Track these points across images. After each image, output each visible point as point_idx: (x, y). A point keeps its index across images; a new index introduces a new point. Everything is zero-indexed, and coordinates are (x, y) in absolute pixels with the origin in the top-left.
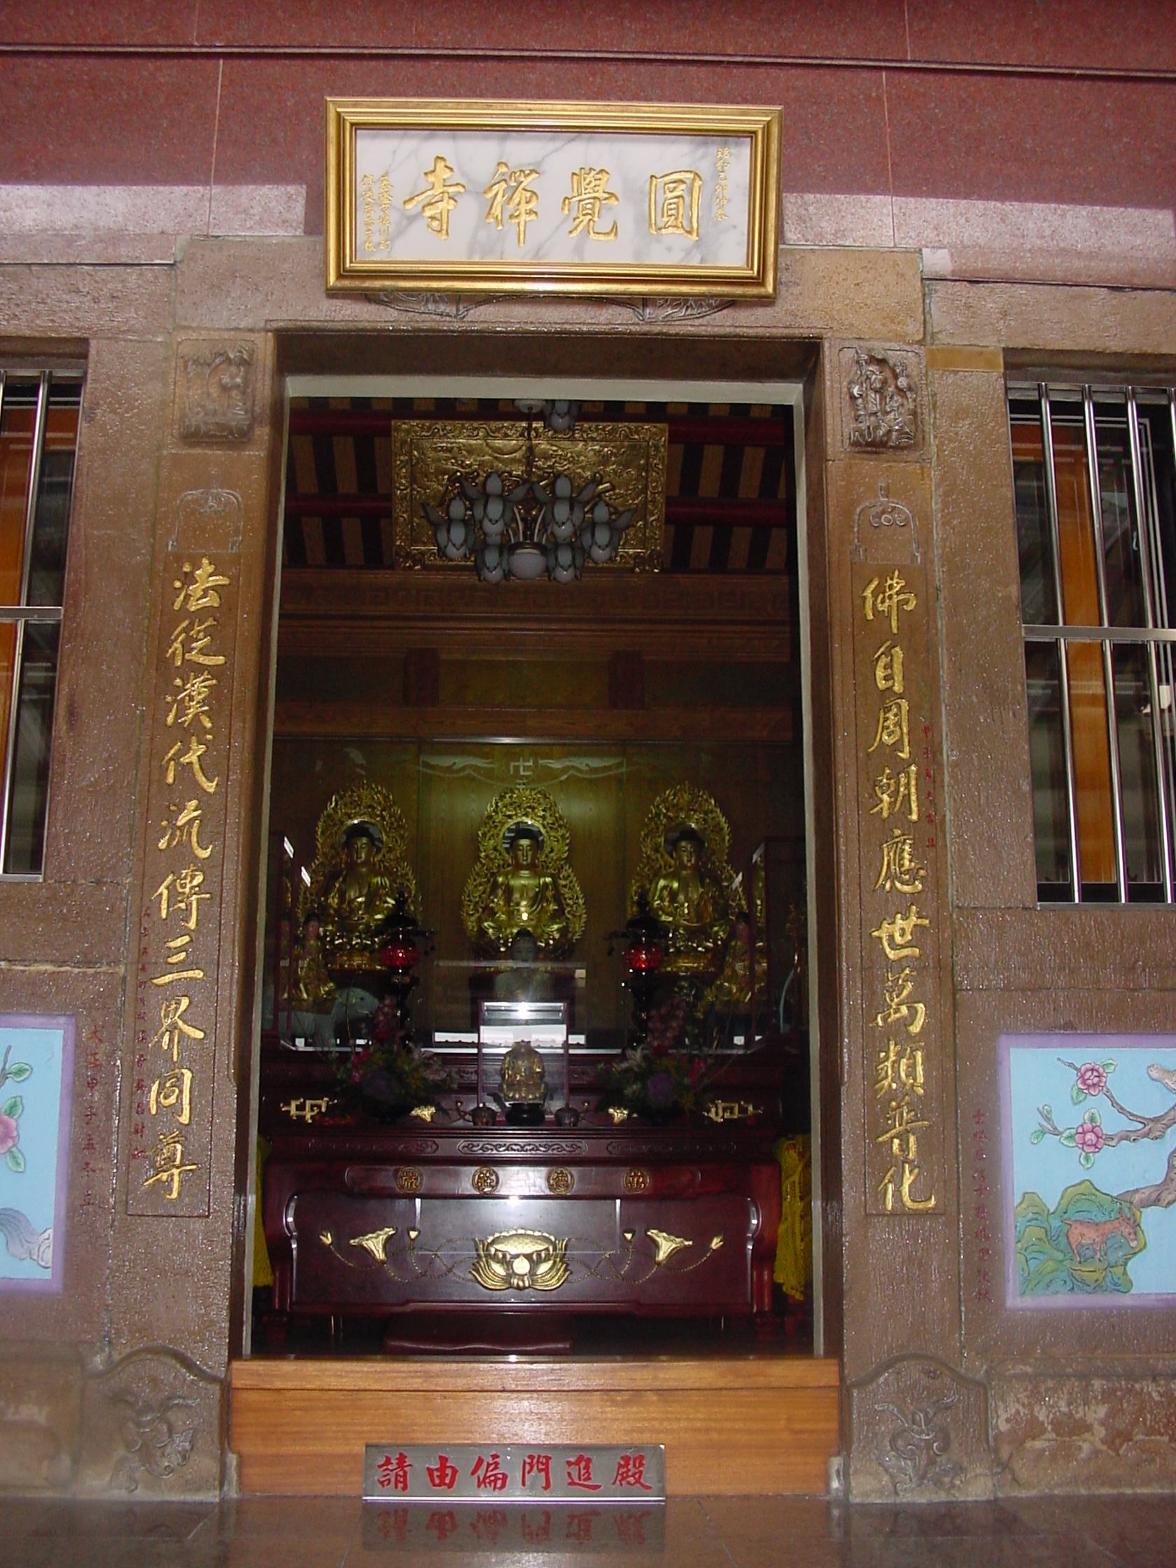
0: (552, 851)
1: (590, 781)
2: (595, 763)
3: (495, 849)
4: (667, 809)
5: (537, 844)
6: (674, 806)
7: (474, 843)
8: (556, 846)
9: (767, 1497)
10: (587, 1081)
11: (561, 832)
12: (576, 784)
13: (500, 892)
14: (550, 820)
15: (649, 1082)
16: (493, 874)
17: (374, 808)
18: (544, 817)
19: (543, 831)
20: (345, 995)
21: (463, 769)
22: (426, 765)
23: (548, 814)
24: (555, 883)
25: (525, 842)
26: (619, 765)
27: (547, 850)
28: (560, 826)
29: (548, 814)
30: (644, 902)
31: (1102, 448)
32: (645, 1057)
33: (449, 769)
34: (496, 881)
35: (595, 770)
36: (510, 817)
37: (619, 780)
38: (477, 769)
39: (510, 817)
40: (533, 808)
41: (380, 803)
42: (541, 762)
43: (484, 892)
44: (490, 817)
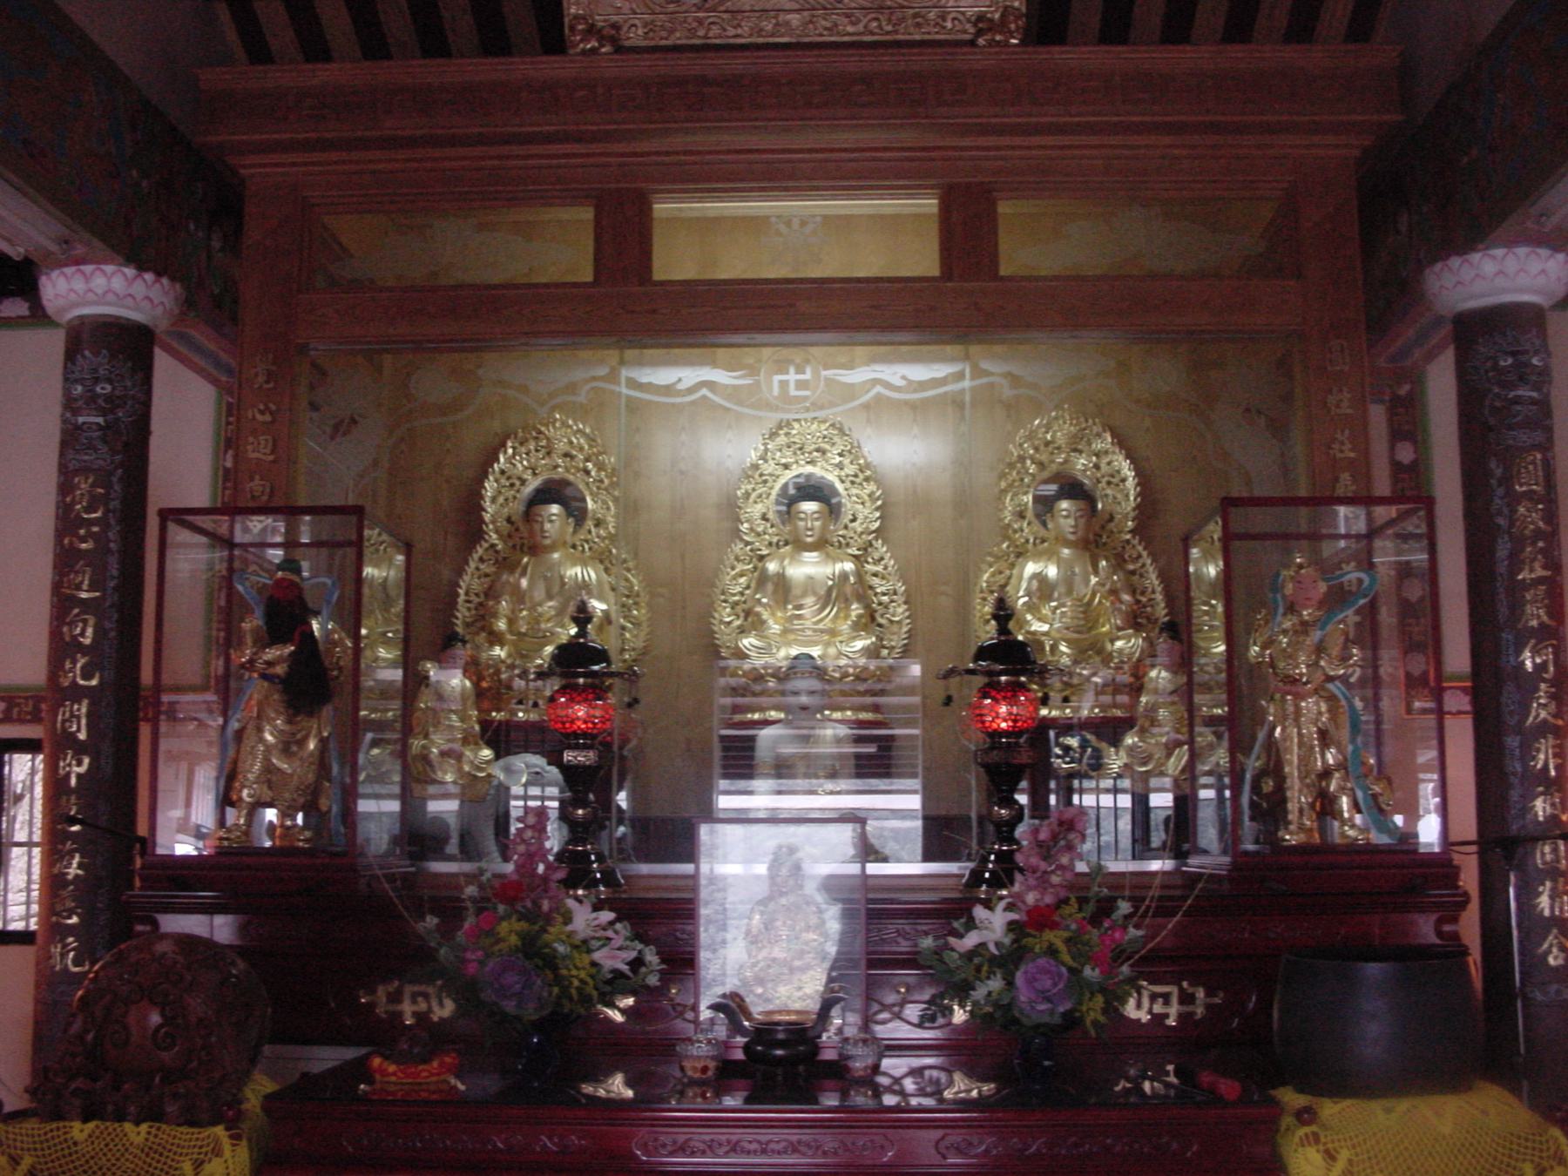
0: (854, 520)
1: (913, 406)
2: (920, 372)
3: (764, 518)
4: (1036, 449)
5: (832, 509)
6: (1047, 444)
7: (731, 509)
8: (860, 509)
9: (1084, 279)
10: (996, 734)
11: (871, 487)
12: (880, 409)
13: (770, 587)
14: (850, 469)
15: (1019, 977)
16: (762, 558)
17: (572, 457)
18: (840, 466)
19: (839, 487)
20: (453, 789)
21: (691, 390)
22: (633, 384)
23: (847, 461)
24: (859, 574)
25: (809, 507)
26: (960, 376)
27: (846, 519)
28: (867, 479)
29: (847, 461)
30: (1003, 614)
31: (688, 868)
32: (1012, 926)
33: (668, 390)
34: (764, 570)
35: (923, 385)
36: (786, 467)
37: (957, 402)
38: (710, 385)
39: (786, 467)
40: (823, 452)
41: (581, 449)
42: (824, 373)
43: (748, 587)
44: (755, 467)
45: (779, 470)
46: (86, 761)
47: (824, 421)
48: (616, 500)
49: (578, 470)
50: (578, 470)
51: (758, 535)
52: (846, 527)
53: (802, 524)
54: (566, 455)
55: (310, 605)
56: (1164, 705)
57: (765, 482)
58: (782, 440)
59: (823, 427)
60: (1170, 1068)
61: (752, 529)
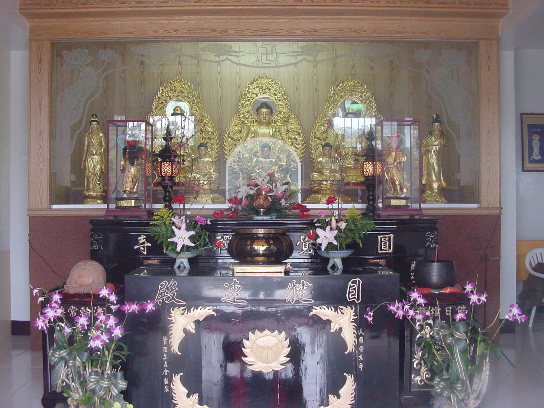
17: (183, 93)
25: (264, 110)
35: (358, 209)
36: (256, 95)
45: (254, 96)
46: (34, 294)
47: (270, 79)
48: (199, 108)
49: (186, 97)
50: (186, 97)
51: (246, 118)
52: (277, 116)
53: (262, 116)
54: (181, 92)
55: (340, 392)
56: (457, 390)
57: (249, 100)
58: (254, 85)
59: (270, 81)
60: (483, 298)
61: (244, 116)
